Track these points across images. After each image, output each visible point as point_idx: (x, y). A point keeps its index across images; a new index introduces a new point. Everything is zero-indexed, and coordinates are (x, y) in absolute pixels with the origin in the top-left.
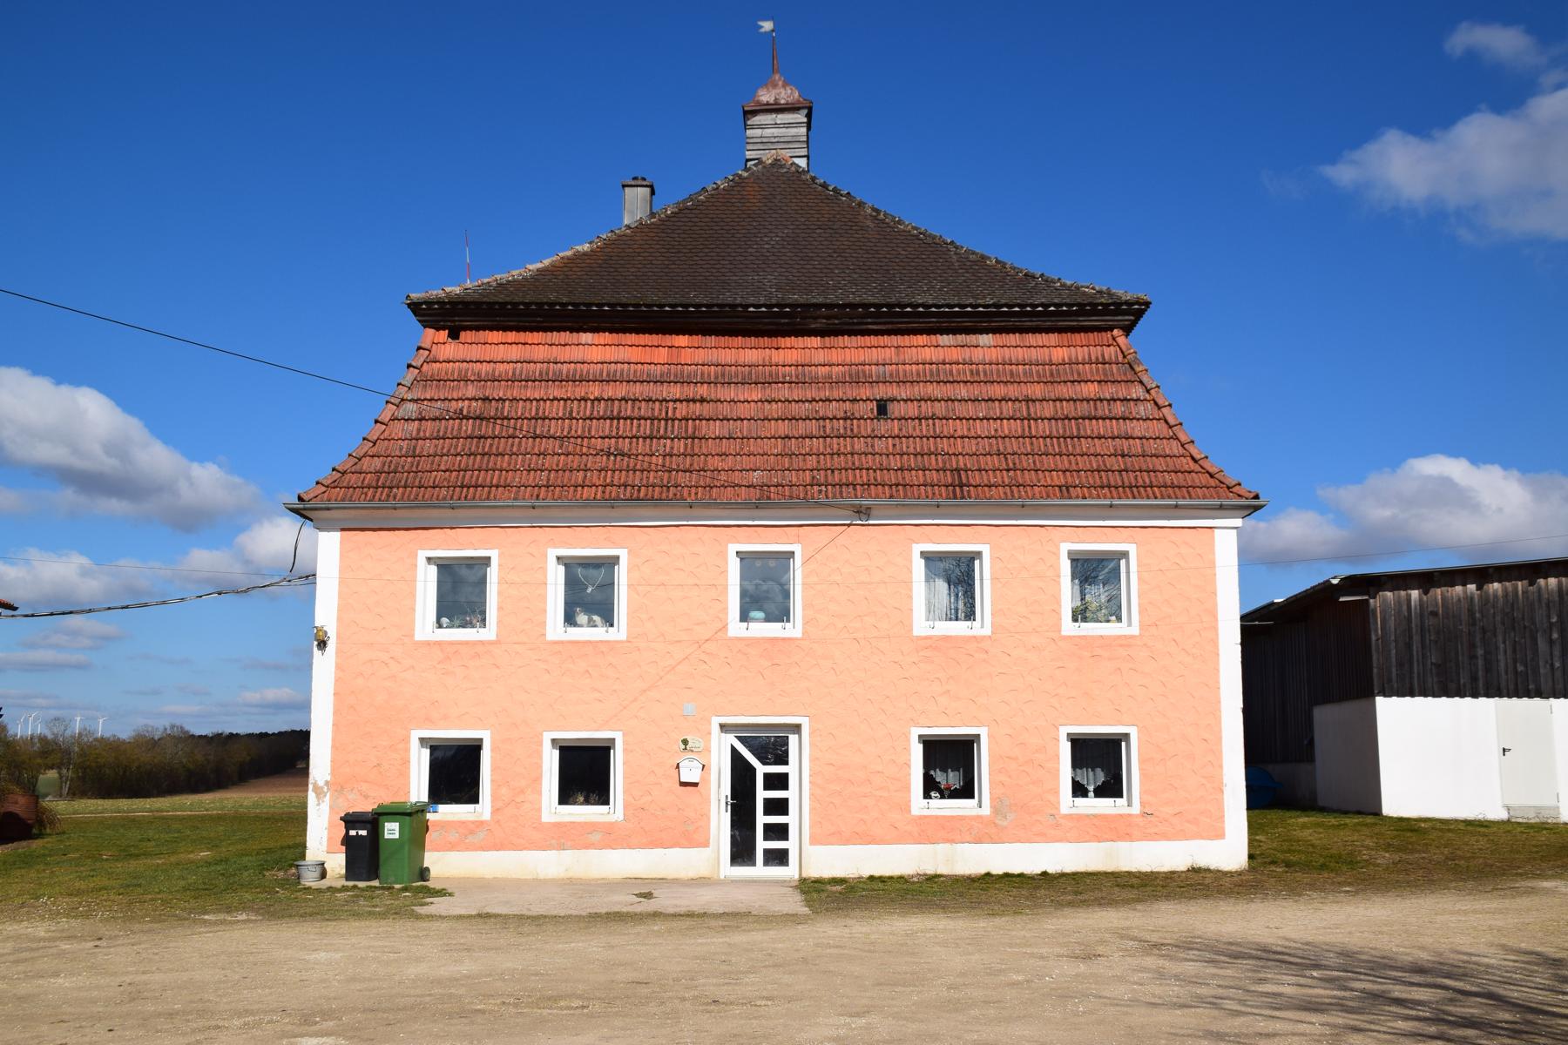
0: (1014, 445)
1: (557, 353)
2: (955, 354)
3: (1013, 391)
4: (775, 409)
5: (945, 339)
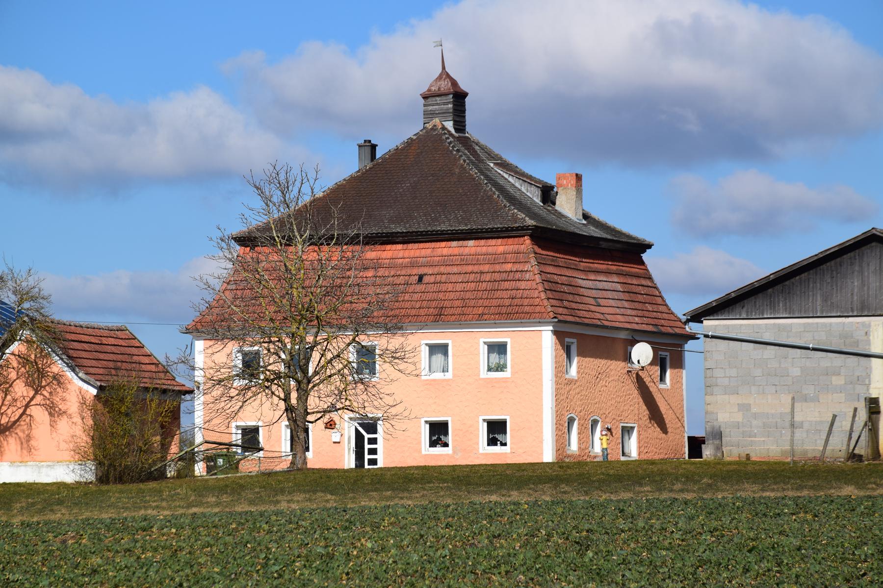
0: (468, 295)
2: (456, 251)
3: (476, 268)
5: (454, 244)
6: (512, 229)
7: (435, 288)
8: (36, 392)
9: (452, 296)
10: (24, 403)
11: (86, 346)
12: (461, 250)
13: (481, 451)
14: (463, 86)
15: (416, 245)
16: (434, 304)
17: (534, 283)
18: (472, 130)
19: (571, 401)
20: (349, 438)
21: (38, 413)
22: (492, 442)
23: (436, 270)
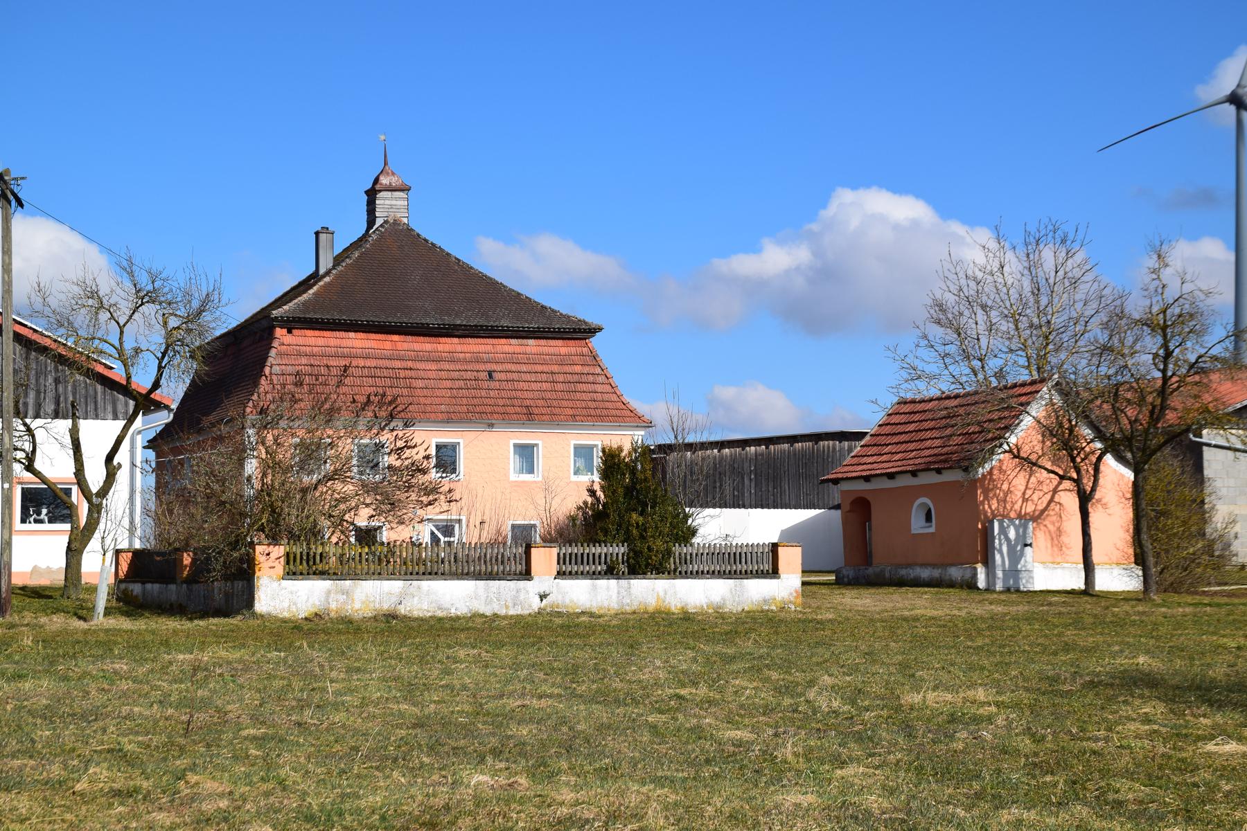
3: (545, 368)
5: (513, 341)
10: (1052, 487)
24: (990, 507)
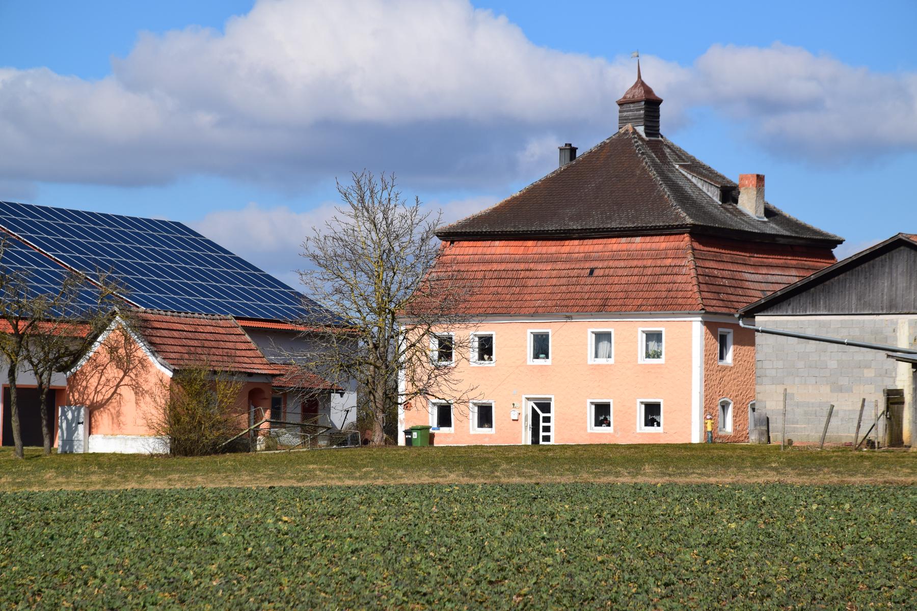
1: (485, 250)
2: (624, 247)
3: (640, 263)
4: (554, 273)
5: (624, 240)
6: (673, 227)
7: (603, 281)
8: (125, 375)
9: (617, 288)
10: (116, 383)
11: (176, 334)
12: (629, 246)
13: (638, 431)
14: (658, 92)
15: (590, 241)
16: (601, 295)
17: (689, 277)
18: (669, 131)
19: (725, 386)
20: (526, 416)
21: (127, 392)
22: (598, 423)
23: (605, 264)
24: (73, 396)
